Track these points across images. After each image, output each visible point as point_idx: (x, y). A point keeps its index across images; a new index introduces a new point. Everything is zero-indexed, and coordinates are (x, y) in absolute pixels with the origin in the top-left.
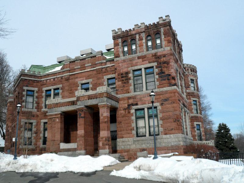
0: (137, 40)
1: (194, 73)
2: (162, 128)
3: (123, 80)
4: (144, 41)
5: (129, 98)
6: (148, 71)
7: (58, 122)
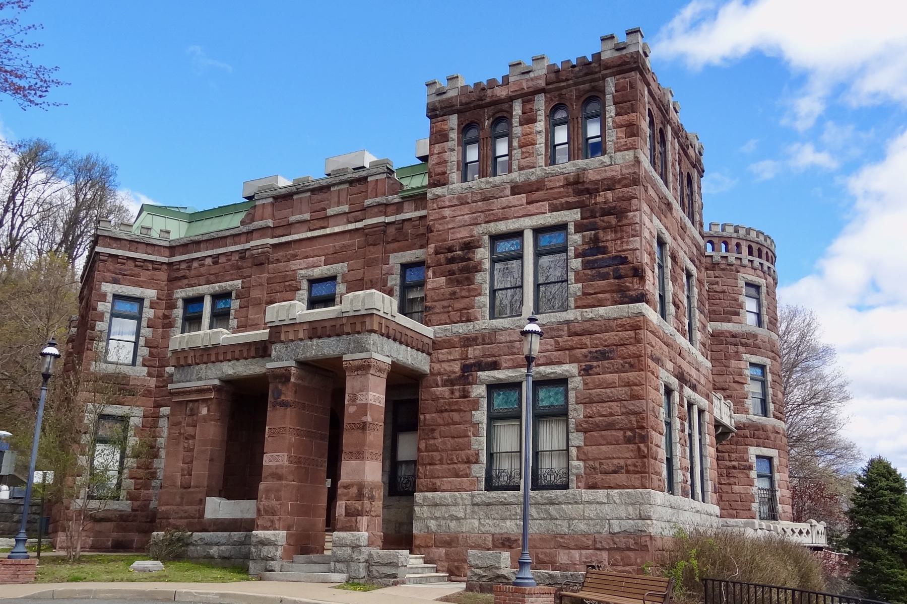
0: (515, 121)
1: (761, 261)
2: (581, 464)
3: (451, 273)
4: (540, 126)
5: (468, 341)
6: (547, 240)
7: (205, 419)
